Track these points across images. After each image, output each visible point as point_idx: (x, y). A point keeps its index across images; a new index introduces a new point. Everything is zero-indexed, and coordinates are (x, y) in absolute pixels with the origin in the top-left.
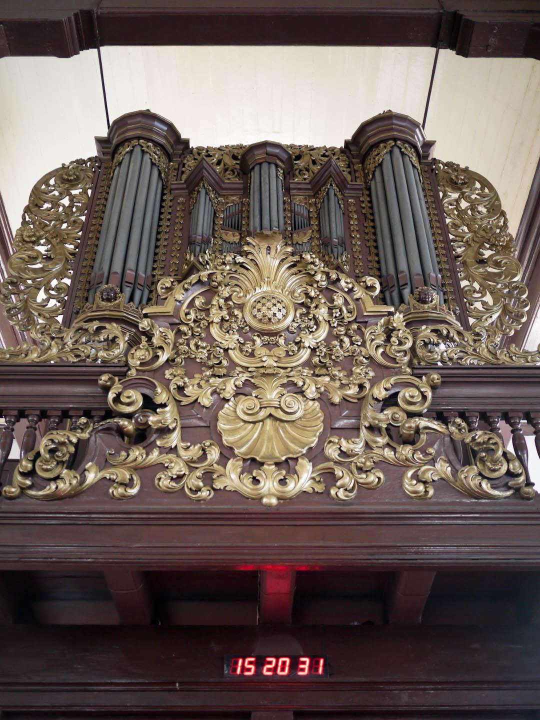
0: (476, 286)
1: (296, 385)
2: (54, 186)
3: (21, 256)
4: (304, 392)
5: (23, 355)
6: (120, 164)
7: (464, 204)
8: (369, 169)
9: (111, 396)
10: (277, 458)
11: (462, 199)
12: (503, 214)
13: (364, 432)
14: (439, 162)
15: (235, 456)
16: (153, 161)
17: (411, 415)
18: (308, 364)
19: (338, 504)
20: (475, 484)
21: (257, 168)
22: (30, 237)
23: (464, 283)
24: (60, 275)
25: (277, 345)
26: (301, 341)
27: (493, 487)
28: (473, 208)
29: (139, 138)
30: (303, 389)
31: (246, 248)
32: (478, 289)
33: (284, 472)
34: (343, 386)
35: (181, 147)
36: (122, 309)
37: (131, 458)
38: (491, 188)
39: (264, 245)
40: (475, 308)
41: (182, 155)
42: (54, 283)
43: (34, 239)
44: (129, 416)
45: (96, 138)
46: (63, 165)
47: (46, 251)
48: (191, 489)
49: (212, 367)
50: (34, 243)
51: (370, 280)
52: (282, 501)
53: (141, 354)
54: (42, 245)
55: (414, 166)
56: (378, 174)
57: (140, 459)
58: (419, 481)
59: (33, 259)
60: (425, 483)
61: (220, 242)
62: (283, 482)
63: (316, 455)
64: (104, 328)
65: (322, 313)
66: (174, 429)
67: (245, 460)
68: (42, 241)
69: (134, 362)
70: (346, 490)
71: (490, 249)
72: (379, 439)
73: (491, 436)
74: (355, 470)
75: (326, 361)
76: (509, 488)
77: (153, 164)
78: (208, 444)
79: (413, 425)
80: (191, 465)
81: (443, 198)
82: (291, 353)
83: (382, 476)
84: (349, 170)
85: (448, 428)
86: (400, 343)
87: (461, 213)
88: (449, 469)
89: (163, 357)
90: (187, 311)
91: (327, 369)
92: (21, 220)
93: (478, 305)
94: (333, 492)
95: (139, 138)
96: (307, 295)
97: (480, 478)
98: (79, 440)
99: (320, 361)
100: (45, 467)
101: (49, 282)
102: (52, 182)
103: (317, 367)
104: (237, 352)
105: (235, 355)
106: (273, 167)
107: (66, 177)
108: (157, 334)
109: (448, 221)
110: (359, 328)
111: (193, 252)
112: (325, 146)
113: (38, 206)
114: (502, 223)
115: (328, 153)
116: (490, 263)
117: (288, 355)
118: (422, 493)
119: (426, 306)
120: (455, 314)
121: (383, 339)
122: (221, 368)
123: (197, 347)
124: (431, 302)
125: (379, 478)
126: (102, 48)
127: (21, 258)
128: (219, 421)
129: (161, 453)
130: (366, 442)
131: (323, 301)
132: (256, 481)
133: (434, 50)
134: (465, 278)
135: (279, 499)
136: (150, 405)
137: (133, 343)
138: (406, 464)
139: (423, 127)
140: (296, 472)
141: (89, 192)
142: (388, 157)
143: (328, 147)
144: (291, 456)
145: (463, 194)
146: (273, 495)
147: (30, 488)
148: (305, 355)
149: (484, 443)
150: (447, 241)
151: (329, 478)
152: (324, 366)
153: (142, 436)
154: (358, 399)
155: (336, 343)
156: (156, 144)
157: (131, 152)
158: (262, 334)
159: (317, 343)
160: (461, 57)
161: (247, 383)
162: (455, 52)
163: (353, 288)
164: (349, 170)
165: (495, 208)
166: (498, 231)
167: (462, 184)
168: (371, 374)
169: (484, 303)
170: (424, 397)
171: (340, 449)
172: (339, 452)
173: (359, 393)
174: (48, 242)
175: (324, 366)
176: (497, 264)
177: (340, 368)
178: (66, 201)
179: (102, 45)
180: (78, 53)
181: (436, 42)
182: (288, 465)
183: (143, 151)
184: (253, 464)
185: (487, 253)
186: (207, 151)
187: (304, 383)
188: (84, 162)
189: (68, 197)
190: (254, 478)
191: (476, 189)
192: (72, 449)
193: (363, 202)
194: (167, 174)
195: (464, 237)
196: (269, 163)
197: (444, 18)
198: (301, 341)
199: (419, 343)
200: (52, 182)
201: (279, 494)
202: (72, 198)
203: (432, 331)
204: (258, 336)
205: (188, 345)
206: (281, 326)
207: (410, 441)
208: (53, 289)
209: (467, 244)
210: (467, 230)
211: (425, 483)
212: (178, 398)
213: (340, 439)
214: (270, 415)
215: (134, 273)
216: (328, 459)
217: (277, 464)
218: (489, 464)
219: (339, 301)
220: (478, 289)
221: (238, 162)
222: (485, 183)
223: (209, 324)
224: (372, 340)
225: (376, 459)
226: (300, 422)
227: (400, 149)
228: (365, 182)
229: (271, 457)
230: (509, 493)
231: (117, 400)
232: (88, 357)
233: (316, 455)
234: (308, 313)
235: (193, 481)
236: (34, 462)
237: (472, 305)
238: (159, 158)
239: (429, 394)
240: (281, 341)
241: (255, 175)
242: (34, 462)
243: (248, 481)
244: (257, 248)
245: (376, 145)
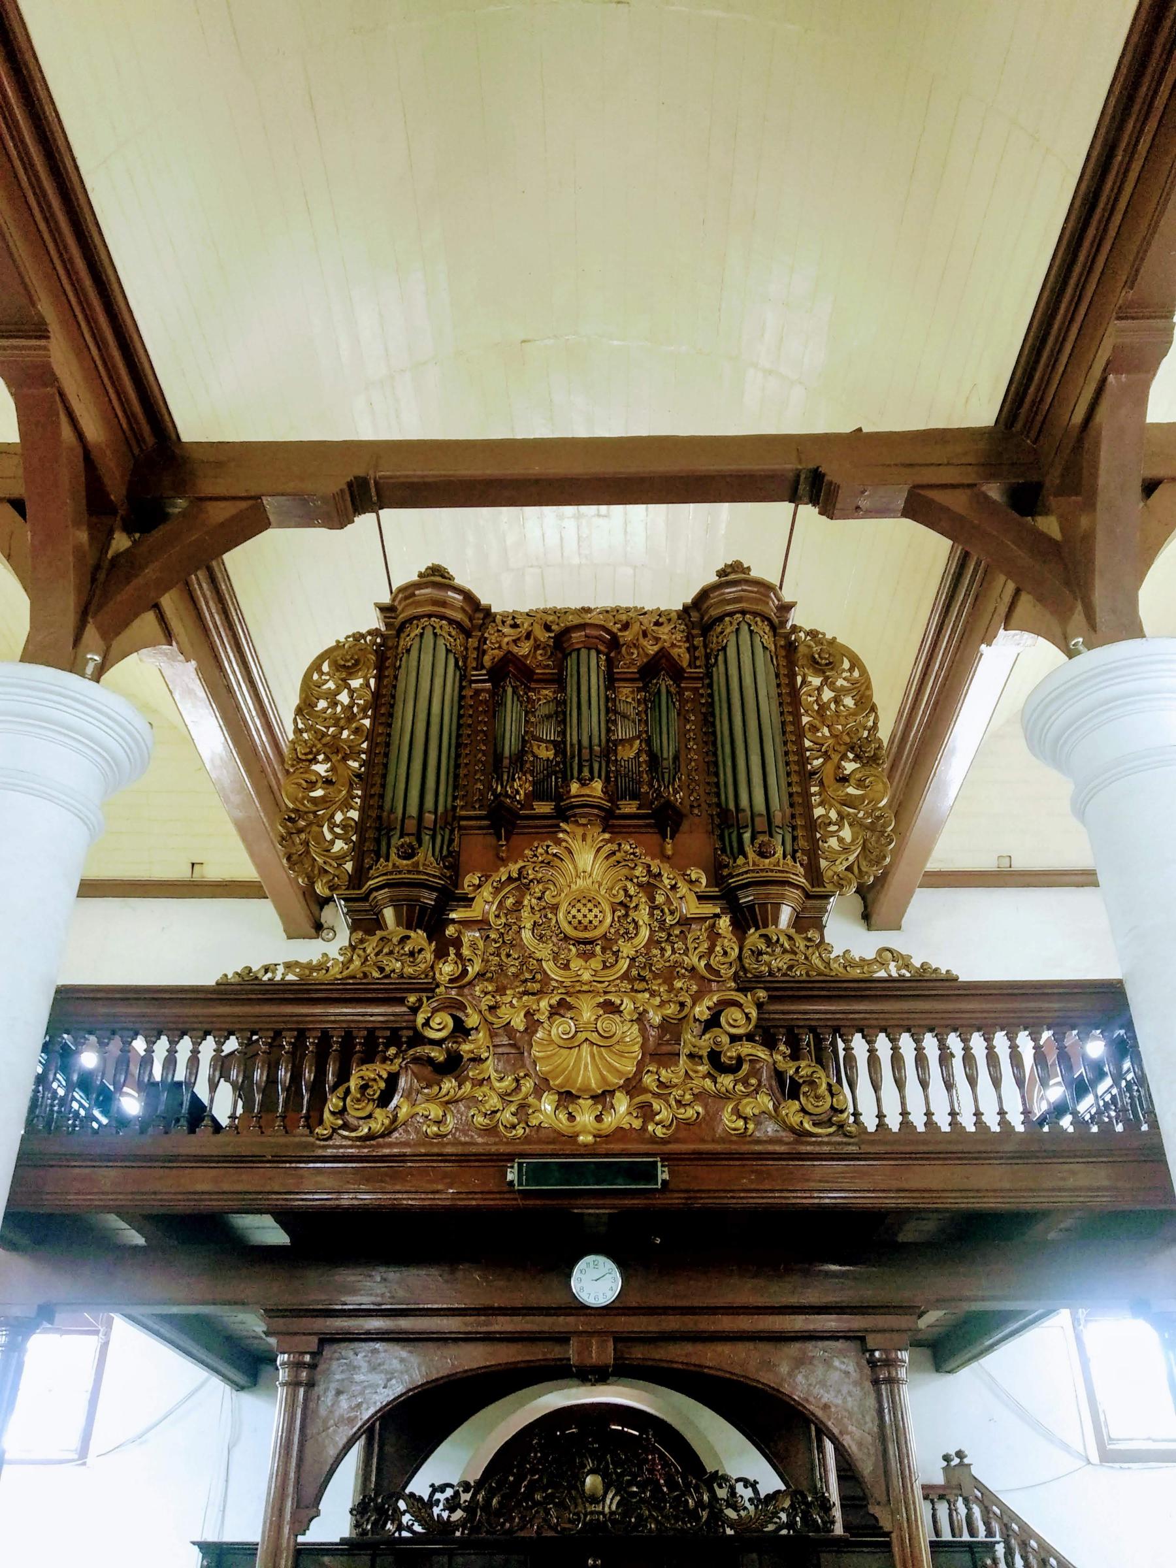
0: (833, 815)
1: (613, 1004)
2: (328, 674)
3: (296, 781)
4: (622, 1012)
5: (324, 971)
6: (408, 651)
7: (827, 695)
8: (712, 650)
9: (420, 1019)
10: (594, 1090)
11: (825, 687)
12: (873, 709)
13: (683, 1059)
14: (801, 629)
15: (550, 1089)
16: (449, 647)
17: (734, 1039)
18: (626, 976)
19: (656, 1143)
20: (795, 1122)
21: (574, 655)
22: (306, 754)
23: (818, 812)
24: (346, 805)
25: (593, 955)
26: (619, 951)
27: (814, 1125)
28: (837, 700)
29: (430, 616)
30: (622, 1008)
31: (561, 835)
32: (834, 820)
33: (600, 1107)
34: (663, 1004)
35: (481, 615)
36: (421, 868)
37: (444, 1091)
38: (864, 672)
39: (579, 831)
40: (829, 847)
41: (482, 627)
42: (339, 817)
43: (310, 757)
44: (438, 1043)
45: (376, 605)
46: (338, 642)
47: (326, 771)
48: (505, 1126)
49: (525, 981)
50: (310, 761)
51: (694, 873)
52: (598, 1139)
53: (447, 969)
54: (321, 763)
55: (765, 648)
56: (721, 658)
57: (452, 1091)
58: (740, 1117)
59: (312, 785)
60: (745, 1119)
61: (531, 759)
62: (599, 1118)
63: (632, 1086)
64: (408, 937)
65: (642, 916)
66: (487, 1058)
67: (560, 1094)
68: (321, 757)
69: (443, 979)
70: (664, 1126)
71: (854, 760)
72: (700, 1068)
73: (815, 1069)
74: (674, 1103)
75: (646, 973)
76: (832, 1125)
77: (448, 651)
78: (522, 1074)
79: (734, 1054)
80: (504, 1096)
81: (801, 686)
82: (608, 964)
83: (700, 1110)
84: (687, 645)
85: (772, 1055)
86: (725, 953)
87: (823, 707)
88: (771, 1103)
89: (472, 971)
90: (496, 913)
91: (647, 982)
92: (293, 727)
93: (833, 842)
94: (650, 1128)
95: (430, 616)
96: (627, 894)
97: (802, 1114)
98: (389, 1073)
99: (639, 974)
100: (356, 1106)
101: (332, 816)
102: (325, 667)
103: (636, 979)
104: (551, 963)
105: (548, 966)
106: (593, 653)
107: (343, 663)
108: (465, 940)
109: (805, 720)
110: (682, 932)
111: (499, 779)
112: (658, 608)
113: (312, 706)
114: (870, 724)
115: (660, 619)
116: (852, 781)
117: (605, 967)
118: (742, 1131)
119: (767, 861)
120: (802, 865)
121: (706, 946)
122: (535, 982)
123: (508, 955)
124: (774, 855)
125: (698, 1113)
126: (381, 512)
127: (296, 784)
128: (534, 1048)
129: (473, 1086)
130: (686, 1071)
131: (643, 900)
132: (571, 1117)
133: (793, 505)
134: (822, 804)
135: (595, 1136)
136: (461, 1030)
137: (441, 954)
138: (725, 1097)
139: (781, 588)
140: (612, 1107)
141: (372, 682)
142: (733, 638)
143: (662, 609)
144: (608, 1088)
145: (826, 679)
146: (590, 1133)
147: (341, 1127)
148: (624, 965)
149: (807, 1076)
150: (802, 750)
151: (646, 1112)
152: (643, 979)
153: (453, 1065)
154: (680, 1020)
155: (656, 952)
156: (451, 621)
157: (422, 635)
158: (578, 942)
159: (637, 951)
160: (824, 518)
161: (562, 1003)
162: (817, 510)
163: (676, 883)
164: (687, 645)
165: (866, 704)
166: (866, 734)
167: (827, 665)
168: (695, 988)
169: (841, 840)
170: (748, 1019)
171: (658, 1080)
172: (657, 1083)
173: (680, 1011)
174: (327, 759)
175: (643, 979)
176: (860, 784)
177: (660, 981)
178: (344, 698)
179: (381, 508)
180: (353, 522)
181: (794, 497)
182: (603, 1098)
183: (435, 635)
184: (567, 1097)
185: (850, 767)
186: (514, 618)
187: (622, 1001)
188: (363, 636)
189: (346, 691)
190: (570, 1114)
191: (844, 670)
192: (382, 1085)
193: (702, 695)
194: (465, 659)
195: (823, 745)
196: (589, 649)
197: (803, 477)
198: (619, 951)
199: (746, 953)
200: (325, 667)
201: (595, 1132)
202: (352, 692)
203: (761, 936)
204: (574, 945)
205: (499, 955)
206: (598, 933)
207: (733, 1069)
208: (338, 826)
209: (826, 756)
210: (827, 734)
211: (745, 1119)
212: (490, 1018)
213: (658, 1068)
214: (587, 1039)
215: (433, 817)
216: (646, 1090)
217: (592, 1097)
218: (812, 1100)
219: (660, 899)
220: (834, 820)
221: (552, 635)
222: (856, 662)
223: (520, 928)
224: (696, 948)
225: (696, 1091)
226: (617, 1047)
227: (750, 626)
228: (706, 666)
229: (586, 1089)
230: (831, 1130)
231: (427, 1023)
232: (393, 971)
233: (632, 1086)
234: (626, 915)
235: (507, 1116)
236: (344, 1099)
237: (826, 842)
238: (455, 640)
239: (754, 1014)
240: (598, 949)
241: (571, 662)
242: (344, 1099)
243: (563, 1117)
244: (571, 835)
245: (720, 619)
